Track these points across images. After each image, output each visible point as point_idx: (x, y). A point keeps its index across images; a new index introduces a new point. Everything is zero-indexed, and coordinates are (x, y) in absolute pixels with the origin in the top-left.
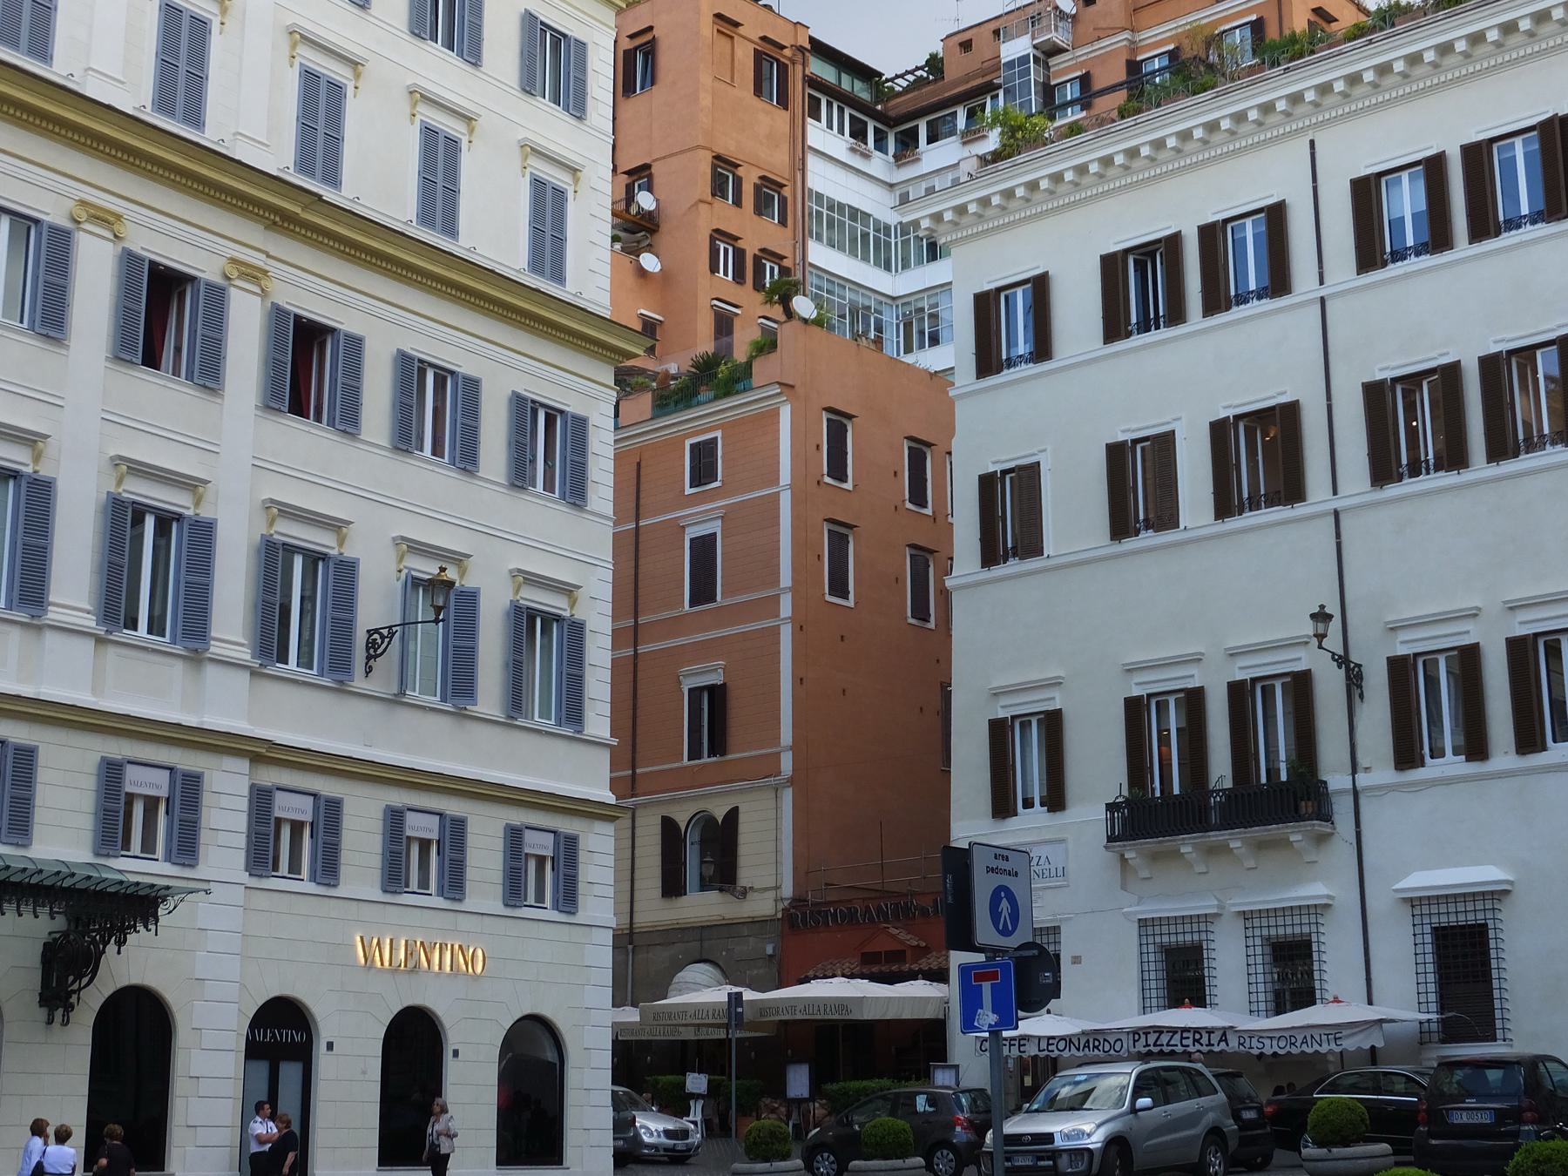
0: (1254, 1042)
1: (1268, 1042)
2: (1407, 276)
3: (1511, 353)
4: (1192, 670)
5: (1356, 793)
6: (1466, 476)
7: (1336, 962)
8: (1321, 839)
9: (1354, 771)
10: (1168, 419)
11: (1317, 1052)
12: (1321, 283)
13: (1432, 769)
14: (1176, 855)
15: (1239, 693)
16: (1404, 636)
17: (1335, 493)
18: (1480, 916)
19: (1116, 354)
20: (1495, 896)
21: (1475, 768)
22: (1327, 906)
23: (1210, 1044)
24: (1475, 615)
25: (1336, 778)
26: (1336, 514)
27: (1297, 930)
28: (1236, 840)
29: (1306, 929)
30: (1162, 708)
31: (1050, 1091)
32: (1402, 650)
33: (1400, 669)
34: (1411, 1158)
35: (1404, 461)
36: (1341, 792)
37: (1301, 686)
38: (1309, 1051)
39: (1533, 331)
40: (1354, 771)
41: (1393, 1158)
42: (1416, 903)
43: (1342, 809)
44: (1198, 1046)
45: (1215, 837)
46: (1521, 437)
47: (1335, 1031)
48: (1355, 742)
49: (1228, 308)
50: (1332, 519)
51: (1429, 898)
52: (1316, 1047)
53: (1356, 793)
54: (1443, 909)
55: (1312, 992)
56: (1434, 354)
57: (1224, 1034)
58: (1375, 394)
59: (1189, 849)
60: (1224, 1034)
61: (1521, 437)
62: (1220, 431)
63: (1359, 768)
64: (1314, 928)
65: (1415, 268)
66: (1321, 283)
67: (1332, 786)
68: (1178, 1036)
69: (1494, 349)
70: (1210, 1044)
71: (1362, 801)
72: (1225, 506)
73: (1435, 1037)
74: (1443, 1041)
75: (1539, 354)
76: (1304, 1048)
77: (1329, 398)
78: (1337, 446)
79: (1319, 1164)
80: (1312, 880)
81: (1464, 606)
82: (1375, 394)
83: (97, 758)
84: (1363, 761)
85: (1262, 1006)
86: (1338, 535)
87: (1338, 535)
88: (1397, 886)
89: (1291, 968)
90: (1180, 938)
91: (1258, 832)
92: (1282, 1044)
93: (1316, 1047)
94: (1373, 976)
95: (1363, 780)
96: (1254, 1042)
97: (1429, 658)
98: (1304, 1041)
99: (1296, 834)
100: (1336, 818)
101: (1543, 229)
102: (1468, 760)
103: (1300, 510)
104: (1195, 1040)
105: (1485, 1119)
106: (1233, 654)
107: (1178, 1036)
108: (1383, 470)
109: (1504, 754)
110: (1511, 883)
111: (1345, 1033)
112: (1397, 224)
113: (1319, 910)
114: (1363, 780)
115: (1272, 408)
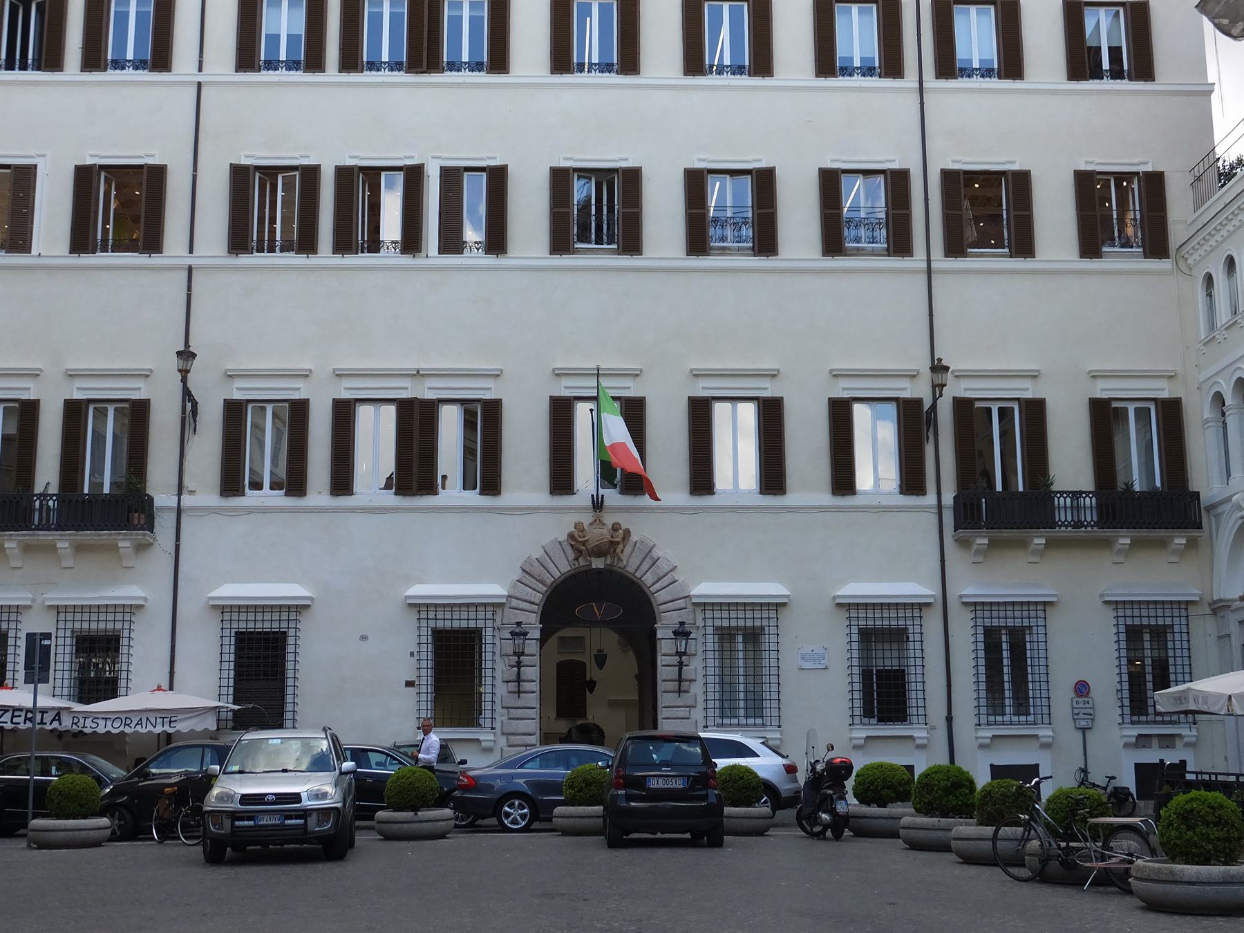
0: (88, 722)
1: (102, 723)
2: (459, 85)
3: (102, 167)
4: (28, 383)
5: (179, 511)
6: (313, 261)
7: (143, 658)
8: (141, 548)
9: (180, 494)
10: (32, 153)
11: (150, 732)
12: (200, 70)
13: (251, 498)
14: (52, 548)
15: (74, 412)
16: (567, 382)
17: (191, 251)
18: (284, 624)
19: (349, 84)
20: (298, 609)
21: (487, 501)
22: (141, 606)
23: (42, 723)
24: (637, 375)
25: (163, 498)
26: (190, 269)
27: (110, 626)
28: (63, 542)
29: (118, 626)
30: (101, 414)
31: (563, 759)
32: (237, 396)
33: (234, 412)
34: (688, 836)
35: (255, 238)
36: (169, 509)
37: (137, 415)
38: (143, 731)
39: (383, 156)
40: (180, 494)
41: (453, 822)
42: (225, 610)
43: (165, 524)
44: (29, 725)
45: (44, 536)
46: (99, 237)
47: (125, 716)
48: (182, 469)
49: (105, 70)
50: (186, 274)
51: (239, 606)
52: (150, 728)
53: (179, 511)
54: (725, 614)
55: (115, 681)
56: (296, 155)
57: (58, 714)
58: (240, 175)
59: (66, 545)
60: (58, 714)
61: (99, 237)
62: (84, 177)
63: (184, 491)
64: (126, 626)
65: (976, 85)
66: (200, 70)
67: (157, 503)
68: (9, 715)
69: (89, 161)
70: (42, 723)
71: (184, 518)
72: (81, 241)
73: (230, 724)
74: (234, 728)
75: (383, 174)
76: (138, 728)
77: (195, 170)
78: (198, 215)
79: (405, 826)
80: (126, 582)
81: (982, 368)
82: (240, 175)
83: (510, 254)
84: (187, 481)
85: (66, 691)
86: (189, 288)
87: (189, 288)
88: (212, 594)
89: (98, 658)
90: (267, 625)
91: (87, 536)
92: (116, 724)
93: (150, 728)
94: (176, 670)
95: (187, 501)
96: (88, 722)
97: (101, 405)
98: (140, 723)
99: (124, 541)
100: (157, 529)
101: (401, 77)
102: (287, 494)
103: (155, 260)
104: (26, 719)
105: (679, 784)
106: (72, 375)
107: (9, 715)
108: (239, 242)
109: (453, 493)
110: (311, 599)
111: (180, 717)
112: (274, 39)
113: (133, 609)
114: (187, 501)
115: (141, 167)
